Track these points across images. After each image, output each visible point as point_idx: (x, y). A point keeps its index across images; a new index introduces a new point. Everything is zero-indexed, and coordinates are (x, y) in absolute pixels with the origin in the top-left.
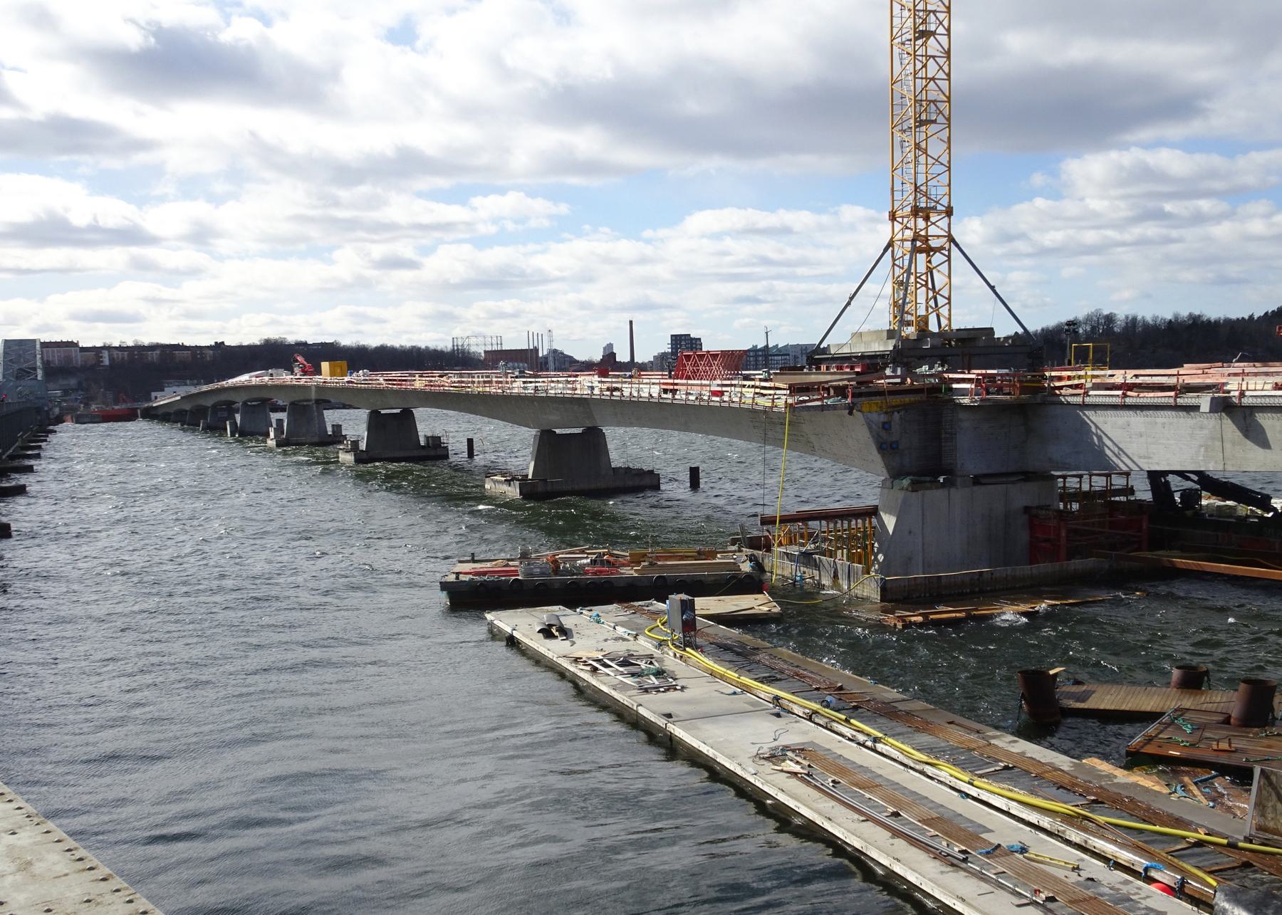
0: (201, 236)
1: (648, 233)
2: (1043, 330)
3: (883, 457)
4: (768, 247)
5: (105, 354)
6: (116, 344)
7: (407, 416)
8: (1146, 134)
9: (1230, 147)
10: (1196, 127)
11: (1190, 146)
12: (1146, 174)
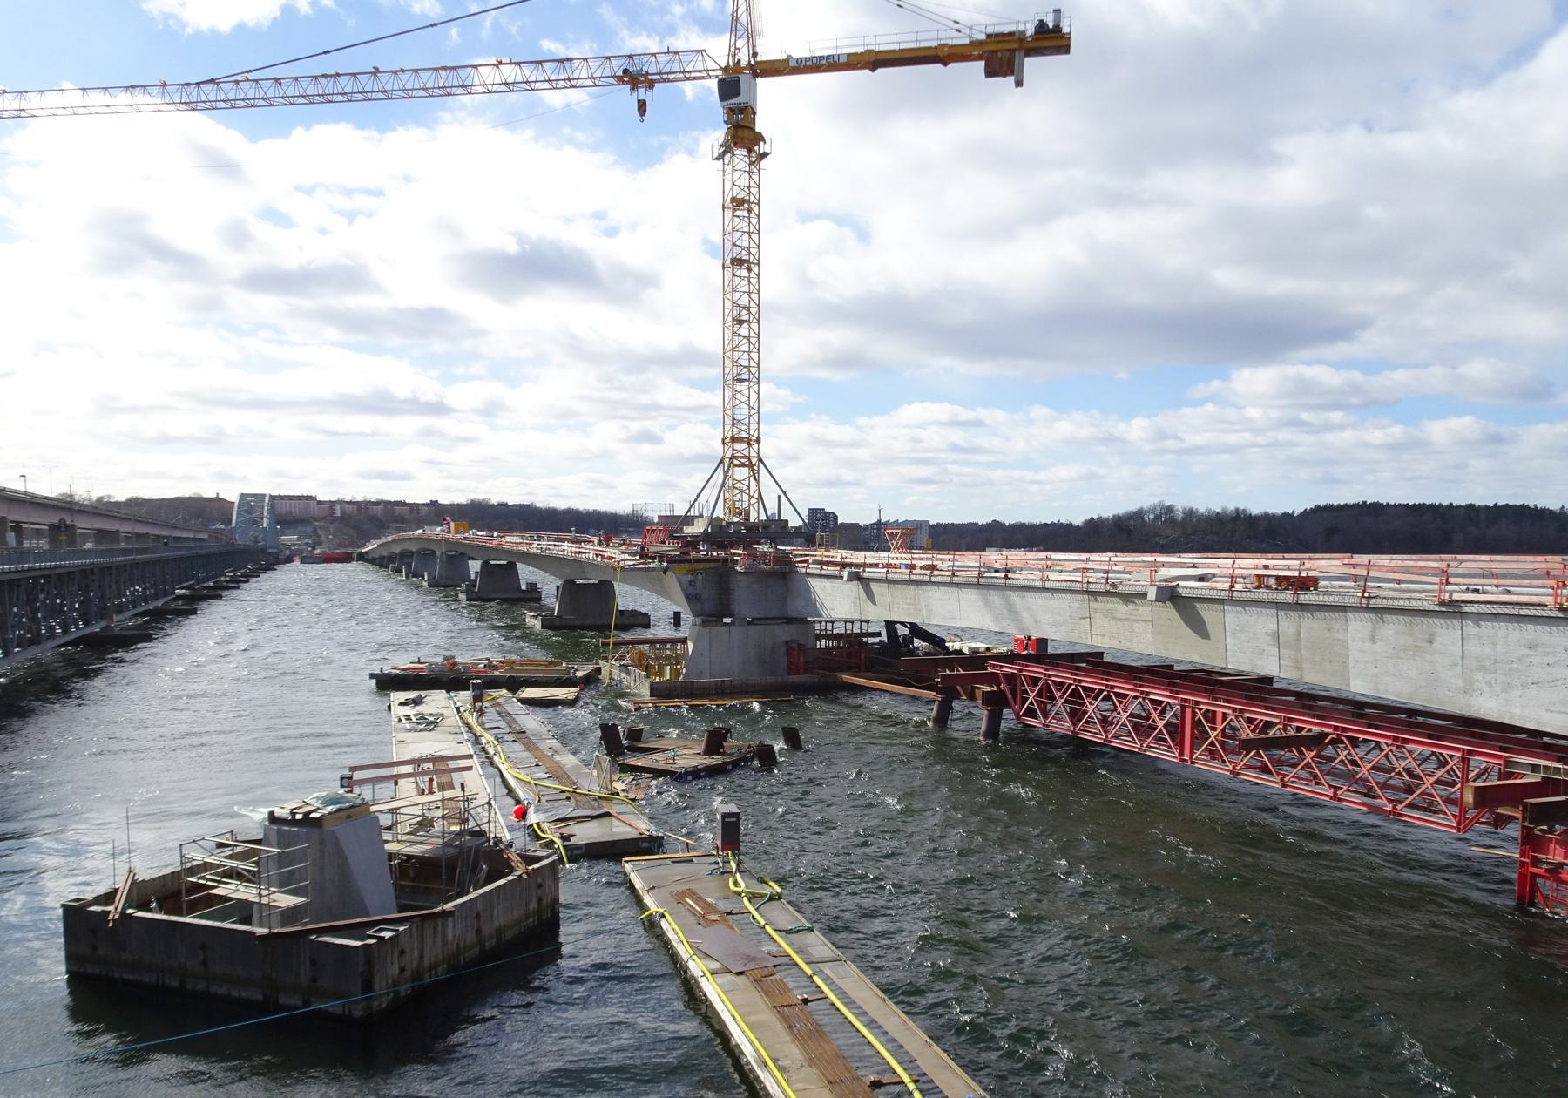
0: (491, 410)
1: (862, 421)
2: (1114, 516)
3: (689, 603)
4: (957, 436)
5: (338, 507)
6: (348, 499)
7: (511, 567)
8: (1306, 354)
9: (1372, 366)
10: (1343, 349)
11: (1340, 365)
12: (1303, 388)
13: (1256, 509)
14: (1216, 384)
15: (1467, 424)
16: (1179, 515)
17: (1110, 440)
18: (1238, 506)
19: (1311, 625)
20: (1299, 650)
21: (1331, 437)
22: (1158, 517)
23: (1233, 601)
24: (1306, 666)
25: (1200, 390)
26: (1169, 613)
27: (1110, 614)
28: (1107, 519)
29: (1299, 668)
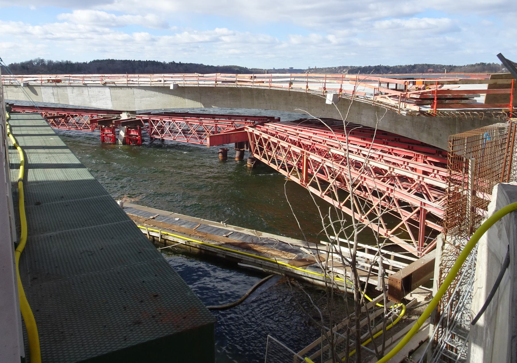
13: (74, 61)
14: (68, 15)
15: (144, 35)
16: (46, 63)
17: (26, 33)
18: (67, 60)
19: (60, 90)
20: (58, 96)
21: (105, 36)
22: (38, 64)
23: (42, 86)
24: (60, 100)
25: (63, 16)
26: (27, 89)
27: (12, 91)
28: (18, 64)
29: (59, 101)
